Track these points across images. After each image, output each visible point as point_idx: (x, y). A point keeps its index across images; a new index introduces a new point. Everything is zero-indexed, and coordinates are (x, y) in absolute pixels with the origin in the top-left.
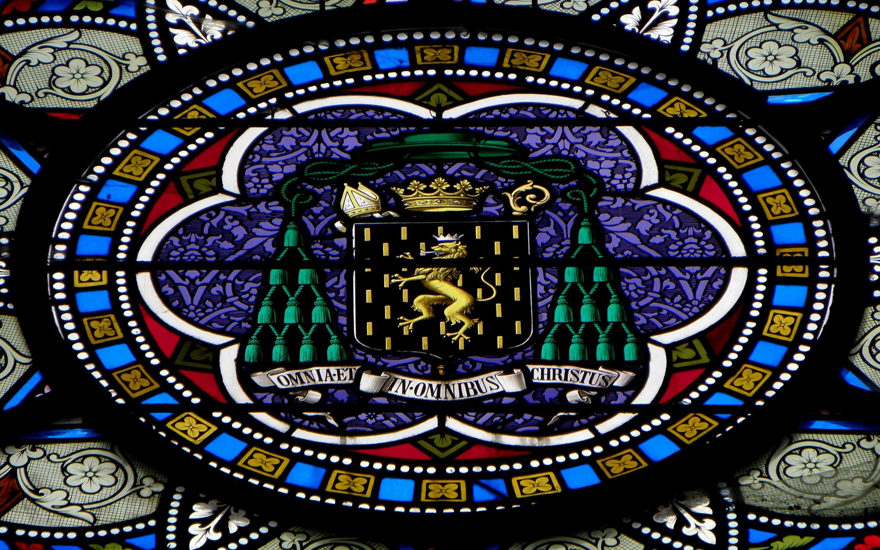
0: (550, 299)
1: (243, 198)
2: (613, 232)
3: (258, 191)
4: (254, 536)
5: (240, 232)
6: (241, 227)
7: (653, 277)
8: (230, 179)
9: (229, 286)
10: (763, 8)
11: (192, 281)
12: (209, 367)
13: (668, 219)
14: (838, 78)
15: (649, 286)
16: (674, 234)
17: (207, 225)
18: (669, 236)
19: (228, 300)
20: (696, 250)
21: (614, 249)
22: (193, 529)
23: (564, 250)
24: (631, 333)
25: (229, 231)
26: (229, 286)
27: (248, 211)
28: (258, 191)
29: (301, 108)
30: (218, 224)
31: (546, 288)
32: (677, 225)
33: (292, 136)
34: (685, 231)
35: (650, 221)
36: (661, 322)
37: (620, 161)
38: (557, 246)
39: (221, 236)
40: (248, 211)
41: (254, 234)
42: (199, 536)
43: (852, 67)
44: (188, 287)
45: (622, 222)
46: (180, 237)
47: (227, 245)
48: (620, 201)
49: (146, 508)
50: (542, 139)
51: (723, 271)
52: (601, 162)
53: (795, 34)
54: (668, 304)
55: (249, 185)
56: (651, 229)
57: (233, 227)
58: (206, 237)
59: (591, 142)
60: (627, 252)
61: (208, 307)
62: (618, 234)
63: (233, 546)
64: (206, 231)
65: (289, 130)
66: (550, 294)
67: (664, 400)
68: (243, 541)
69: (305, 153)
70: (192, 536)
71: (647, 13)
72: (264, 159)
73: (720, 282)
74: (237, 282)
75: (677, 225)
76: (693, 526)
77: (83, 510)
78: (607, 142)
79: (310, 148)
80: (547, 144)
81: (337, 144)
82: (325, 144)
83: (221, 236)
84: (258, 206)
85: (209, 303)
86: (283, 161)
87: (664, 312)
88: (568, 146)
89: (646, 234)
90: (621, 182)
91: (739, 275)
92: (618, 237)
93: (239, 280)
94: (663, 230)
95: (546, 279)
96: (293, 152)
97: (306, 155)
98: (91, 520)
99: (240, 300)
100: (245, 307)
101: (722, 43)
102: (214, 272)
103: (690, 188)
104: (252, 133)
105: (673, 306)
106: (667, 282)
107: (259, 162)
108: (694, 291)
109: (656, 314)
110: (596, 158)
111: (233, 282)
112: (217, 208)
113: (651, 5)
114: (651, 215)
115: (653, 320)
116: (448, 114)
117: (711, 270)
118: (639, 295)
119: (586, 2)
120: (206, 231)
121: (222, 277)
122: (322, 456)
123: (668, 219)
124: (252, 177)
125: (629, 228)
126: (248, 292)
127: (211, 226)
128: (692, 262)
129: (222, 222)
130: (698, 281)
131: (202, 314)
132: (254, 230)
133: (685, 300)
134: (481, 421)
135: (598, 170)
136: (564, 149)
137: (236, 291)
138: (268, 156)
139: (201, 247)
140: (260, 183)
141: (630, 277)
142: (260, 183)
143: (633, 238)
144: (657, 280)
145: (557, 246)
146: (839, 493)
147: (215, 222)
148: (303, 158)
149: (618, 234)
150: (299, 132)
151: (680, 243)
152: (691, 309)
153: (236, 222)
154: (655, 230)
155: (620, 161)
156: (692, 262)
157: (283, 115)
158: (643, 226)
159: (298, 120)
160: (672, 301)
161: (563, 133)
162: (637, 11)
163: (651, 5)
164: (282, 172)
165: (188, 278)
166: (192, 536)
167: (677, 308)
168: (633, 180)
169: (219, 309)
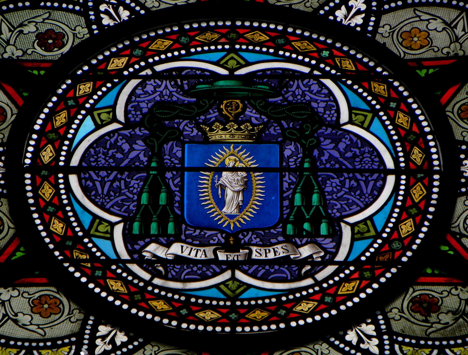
0: (291, 191)
1: (128, 124)
2: (325, 149)
3: (135, 119)
4: (130, 347)
5: (126, 147)
6: (126, 144)
7: (345, 179)
8: (120, 114)
9: (123, 182)
10: (413, 5)
11: (103, 178)
12: (108, 236)
13: (355, 141)
14: (453, 52)
15: (343, 183)
16: (357, 151)
17: (109, 142)
18: (355, 152)
19: (122, 191)
20: (369, 161)
21: (326, 160)
22: (98, 342)
23: (299, 160)
24: (172, 215)
25: (121, 146)
26: (123, 182)
27: (130, 133)
28: (135, 119)
29: (159, 68)
30: (115, 141)
31: (290, 184)
32: (360, 145)
33: (151, 84)
34: (364, 149)
35: (345, 142)
36: (348, 207)
37: (329, 103)
38: (295, 158)
39: (116, 150)
40: (130, 133)
41: (134, 148)
42: (101, 346)
43: (461, 44)
44: (100, 182)
45: (330, 143)
46: (94, 148)
47: (119, 155)
48: (329, 130)
49: (76, 327)
50: (154, 88)
51: (382, 175)
52: (318, 103)
53: (430, 23)
54: (352, 196)
55: (130, 116)
56: (346, 147)
57: (123, 144)
58: (109, 150)
59: (313, 91)
60: (137, 164)
61: (112, 196)
62: (329, 151)
63: (119, 352)
64: (108, 147)
65: (150, 81)
66: (291, 189)
67: (351, 259)
68: (125, 350)
69: (159, 95)
70: (97, 346)
71: (349, 9)
72: (137, 99)
73: (381, 182)
74: (127, 179)
75: (360, 145)
76: (366, 343)
77: (39, 328)
78: (321, 90)
79: (162, 92)
80: (157, 91)
81: (307, 89)
82: (301, 89)
83: (116, 150)
84: (270, 130)
85: (112, 193)
86: (148, 100)
87: (350, 201)
88: (301, 93)
89: (343, 151)
90: (329, 116)
91: (391, 179)
92: (328, 152)
93: (128, 178)
94: (352, 149)
95: (290, 179)
96: (153, 94)
97: (160, 97)
98: (43, 334)
99: (129, 191)
100: (131, 196)
101: (389, 27)
102: (115, 173)
103: (366, 125)
104: (134, 83)
105: (355, 197)
106: (89, 183)
107: (135, 101)
108: (103, 189)
109: (346, 202)
110: (316, 101)
111: (125, 180)
112: (114, 132)
113: (350, 3)
114: (346, 139)
115: (345, 206)
116: (237, 73)
117: (376, 176)
118: (337, 189)
119: (318, 2)
120: (108, 147)
121: (119, 176)
122: (170, 295)
123: (355, 141)
124: (131, 111)
125: (334, 147)
126: (133, 186)
127: (111, 142)
128: (103, 168)
129: (116, 141)
130: (106, 182)
131: (108, 200)
132: (134, 146)
133: (362, 194)
134: (250, 271)
135: (317, 108)
136: (299, 95)
137: (127, 185)
138: (139, 97)
139: (106, 157)
140: (135, 114)
141: (333, 178)
142: (135, 114)
143: (336, 154)
144: (347, 181)
145: (295, 158)
146: (442, 322)
147: (113, 140)
148: (158, 98)
149: (329, 151)
150: (155, 82)
151: (361, 157)
152: (365, 199)
153: (124, 141)
154: (348, 148)
155: (329, 103)
156: (103, 168)
157: (149, 72)
158: (342, 146)
159: (156, 75)
160: (355, 194)
161: (298, 84)
162: (343, 8)
163: (350, 3)
164: (147, 107)
165: (100, 176)
166: (97, 346)
167: (357, 199)
168: (335, 115)
169: (118, 197)
